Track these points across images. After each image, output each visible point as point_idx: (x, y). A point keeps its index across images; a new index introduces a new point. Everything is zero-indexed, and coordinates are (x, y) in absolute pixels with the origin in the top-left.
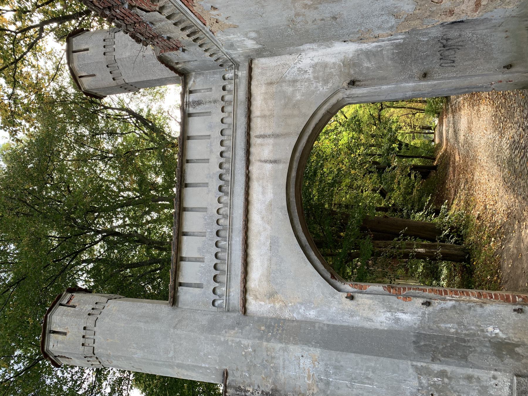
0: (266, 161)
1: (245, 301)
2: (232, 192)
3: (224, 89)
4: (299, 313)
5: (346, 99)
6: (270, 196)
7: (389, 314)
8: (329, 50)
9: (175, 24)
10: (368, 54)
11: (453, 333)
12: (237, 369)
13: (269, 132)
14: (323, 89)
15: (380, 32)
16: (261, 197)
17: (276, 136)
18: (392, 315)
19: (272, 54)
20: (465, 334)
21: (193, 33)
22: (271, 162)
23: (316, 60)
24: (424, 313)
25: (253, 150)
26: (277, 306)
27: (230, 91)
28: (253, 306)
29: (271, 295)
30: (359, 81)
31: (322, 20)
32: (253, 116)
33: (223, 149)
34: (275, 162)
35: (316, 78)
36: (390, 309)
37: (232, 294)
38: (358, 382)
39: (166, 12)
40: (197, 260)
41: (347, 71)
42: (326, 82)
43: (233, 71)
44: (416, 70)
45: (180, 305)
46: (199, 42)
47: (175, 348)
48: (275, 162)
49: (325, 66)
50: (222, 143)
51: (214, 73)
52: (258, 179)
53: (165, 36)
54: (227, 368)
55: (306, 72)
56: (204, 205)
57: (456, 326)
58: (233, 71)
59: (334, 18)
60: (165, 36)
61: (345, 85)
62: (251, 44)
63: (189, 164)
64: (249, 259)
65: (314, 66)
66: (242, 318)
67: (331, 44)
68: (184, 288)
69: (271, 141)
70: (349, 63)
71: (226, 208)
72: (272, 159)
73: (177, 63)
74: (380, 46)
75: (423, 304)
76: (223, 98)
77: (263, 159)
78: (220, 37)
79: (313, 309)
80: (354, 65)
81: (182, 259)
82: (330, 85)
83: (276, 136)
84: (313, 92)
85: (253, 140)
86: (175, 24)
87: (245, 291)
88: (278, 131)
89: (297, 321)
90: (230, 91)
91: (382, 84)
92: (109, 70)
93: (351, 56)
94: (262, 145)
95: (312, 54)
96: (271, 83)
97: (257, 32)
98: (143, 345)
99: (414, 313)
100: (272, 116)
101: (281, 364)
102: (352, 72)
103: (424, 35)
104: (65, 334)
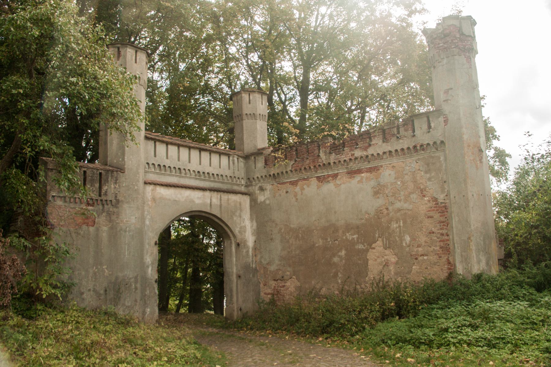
0: (211, 200)
6: (197, 201)
7: (150, 263)
8: (250, 234)
13: (222, 202)
14: (236, 231)
16: (197, 196)
17: (221, 206)
19: (251, 207)
23: (247, 227)
24: (152, 280)
25: (216, 193)
26: (150, 203)
27: (237, 181)
28: (149, 188)
29: (154, 199)
34: (211, 205)
36: (152, 263)
37: (151, 175)
39: (289, 172)
42: (240, 232)
44: (241, 273)
48: (211, 205)
49: (245, 232)
52: (203, 195)
56: (191, 161)
61: (238, 241)
63: (209, 155)
65: (245, 227)
68: (153, 145)
69: (219, 203)
70: (245, 242)
76: (235, 177)
82: (238, 234)
83: (221, 206)
85: (219, 194)
88: (222, 207)
92: (252, 114)
94: (217, 198)
96: (240, 204)
97: (269, 205)
99: (151, 274)
100: (228, 204)
101: (131, 206)
104: (136, 62)
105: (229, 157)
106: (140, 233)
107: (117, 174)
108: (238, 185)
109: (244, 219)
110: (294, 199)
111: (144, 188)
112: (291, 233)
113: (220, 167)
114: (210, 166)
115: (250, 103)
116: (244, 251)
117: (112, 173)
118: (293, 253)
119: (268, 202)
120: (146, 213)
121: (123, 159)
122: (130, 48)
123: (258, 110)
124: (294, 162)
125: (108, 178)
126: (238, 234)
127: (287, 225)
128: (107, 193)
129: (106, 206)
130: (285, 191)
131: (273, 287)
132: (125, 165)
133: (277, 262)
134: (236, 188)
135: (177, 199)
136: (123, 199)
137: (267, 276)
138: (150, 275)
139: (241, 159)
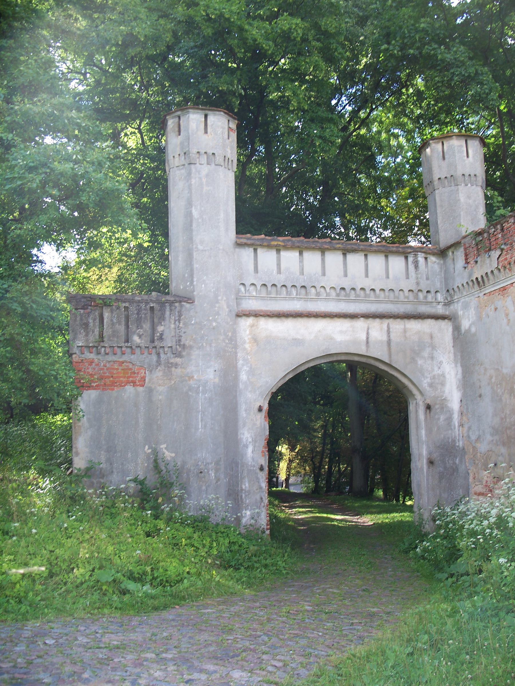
0: (368, 333)
1: (248, 314)
2: (340, 300)
3: (428, 292)
4: (243, 365)
5: (415, 402)
6: (339, 338)
7: (250, 440)
8: (454, 387)
9: (487, 273)
10: (449, 419)
11: (241, 487)
12: (196, 313)
13: (392, 335)
14: (425, 384)
15: (466, 428)
18: (250, 442)
20: (242, 496)
21: (478, 283)
22: (367, 338)
23: (447, 376)
25: (378, 320)
26: (247, 346)
27: (426, 297)
28: (245, 323)
29: (255, 340)
30: (430, 412)
31: (480, 387)
32: (406, 321)
33: (378, 291)
34: (367, 342)
35: (434, 377)
36: (254, 441)
37: (250, 301)
38: (201, 417)
39: (496, 272)
40: (279, 265)
41: (438, 402)
42: (431, 385)
43: (442, 300)
44: (435, 456)
45: (237, 250)
46: (471, 284)
47: (205, 251)
49: (443, 384)
50: (382, 290)
51: (441, 282)
53: (479, 259)
54: (196, 303)
55: (439, 368)
57: (247, 489)
58: (442, 300)
59: (480, 396)
60: (479, 259)
61: (428, 401)
62: (465, 324)
63: (363, 257)
64: (284, 319)
66: (234, 314)
67: (460, 390)
68: (252, 254)
69: (385, 338)
70: (443, 403)
71: (325, 295)
72: (370, 339)
73: (453, 252)
74: (455, 428)
75: (262, 465)
76: (420, 291)
77: (370, 331)
78: (474, 302)
79: (248, 378)
80: (442, 408)
81: (278, 251)
82: (428, 388)
84: (423, 375)
85: (386, 322)
86: (487, 273)
87: (257, 315)
89: (237, 363)
90: (426, 297)
91: (426, 430)
93: (449, 405)
94: (381, 329)
95: (453, 373)
96: (432, 337)
98: (204, 217)
99: (253, 459)
102: (437, 406)
103: (461, 461)
104: (206, 132)
105: (406, 258)
106: (228, 392)
107: (182, 306)
108: (427, 303)
109: (441, 363)
110: (505, 321)
111: (235, 323)
112: (504, 383)
113: (388, 277)
114: (367, 276)
115: (444, 158)
116: (442, 418)
117: (170, 306)
118: (508, 420)
119: (473, 330)
120: (240, 362)
121: (192, 282)
122: (194, 113)
123: (459, 168)
124: (498, 252)
125: (163, 314)
126: (428, 388)
127: (498, 369)
128: (163, 337)
129: (162, 356)
130: (493, 307)
131: (484, 482)
132: (194, 291)
133: (489, 437)
134: (423, 309)
135: (299, 337)
136: (191, 343)
137: (477, 462)
138: (250, 459)
139: (432, 259)
